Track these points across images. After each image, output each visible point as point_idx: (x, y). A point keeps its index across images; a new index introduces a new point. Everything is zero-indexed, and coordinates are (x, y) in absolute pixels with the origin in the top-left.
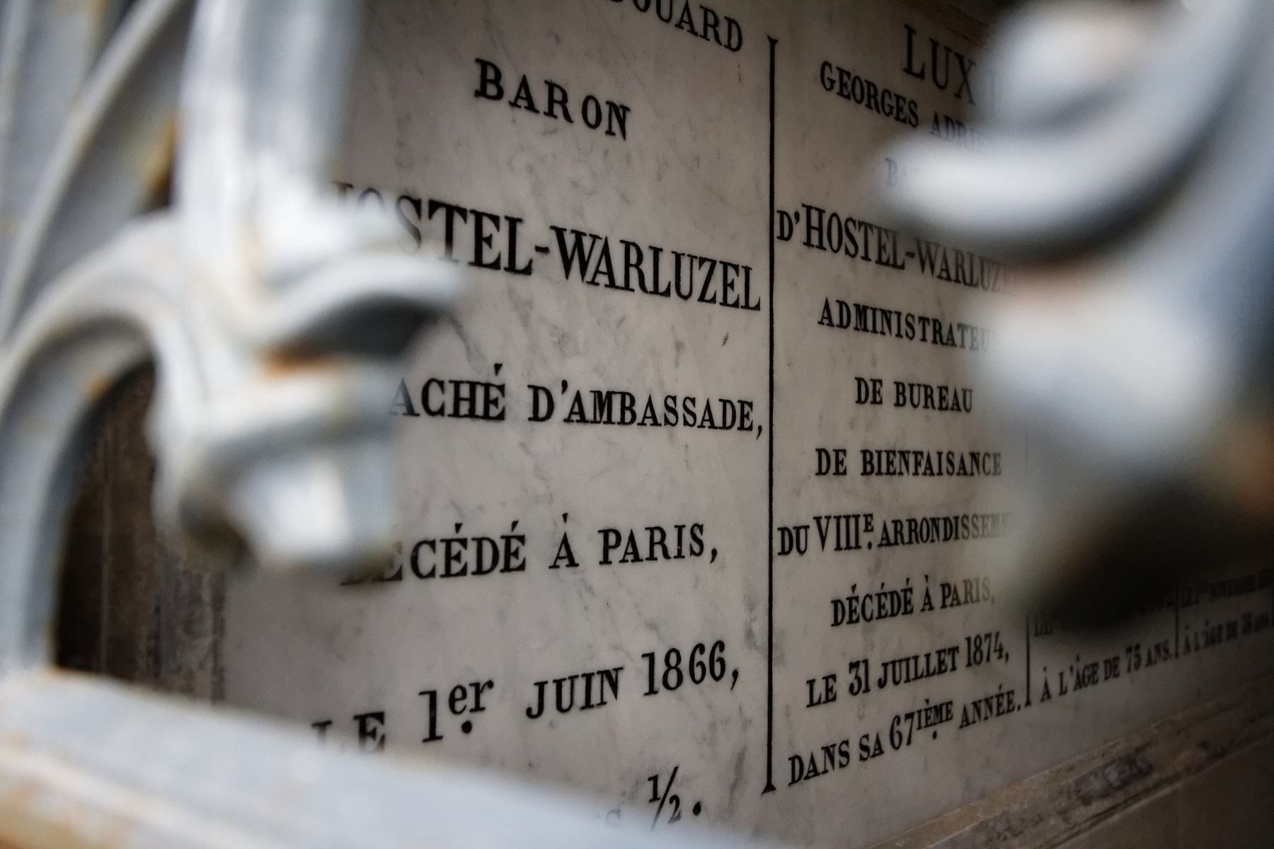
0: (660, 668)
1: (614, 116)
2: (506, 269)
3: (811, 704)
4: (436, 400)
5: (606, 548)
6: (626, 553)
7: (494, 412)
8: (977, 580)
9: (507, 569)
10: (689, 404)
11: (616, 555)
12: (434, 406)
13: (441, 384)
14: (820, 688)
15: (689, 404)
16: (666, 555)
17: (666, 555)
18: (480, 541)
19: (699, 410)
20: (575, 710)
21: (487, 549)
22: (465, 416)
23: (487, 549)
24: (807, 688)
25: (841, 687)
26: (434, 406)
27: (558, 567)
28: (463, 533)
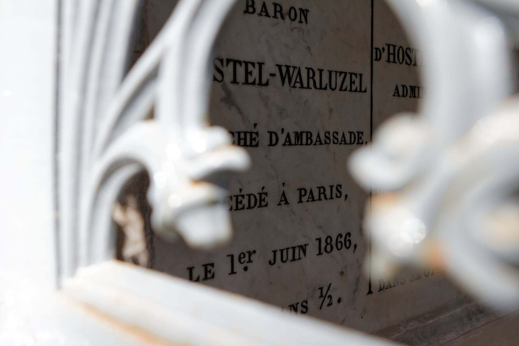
0: (323, 244)
5: (301, 196)
6: (309, 198)
7: (254, 143)
10: (335, 135)
11: (304, 199)
15: (335, 135)
16: (326, 198)
17: (326, 198)
19: (340, 137)
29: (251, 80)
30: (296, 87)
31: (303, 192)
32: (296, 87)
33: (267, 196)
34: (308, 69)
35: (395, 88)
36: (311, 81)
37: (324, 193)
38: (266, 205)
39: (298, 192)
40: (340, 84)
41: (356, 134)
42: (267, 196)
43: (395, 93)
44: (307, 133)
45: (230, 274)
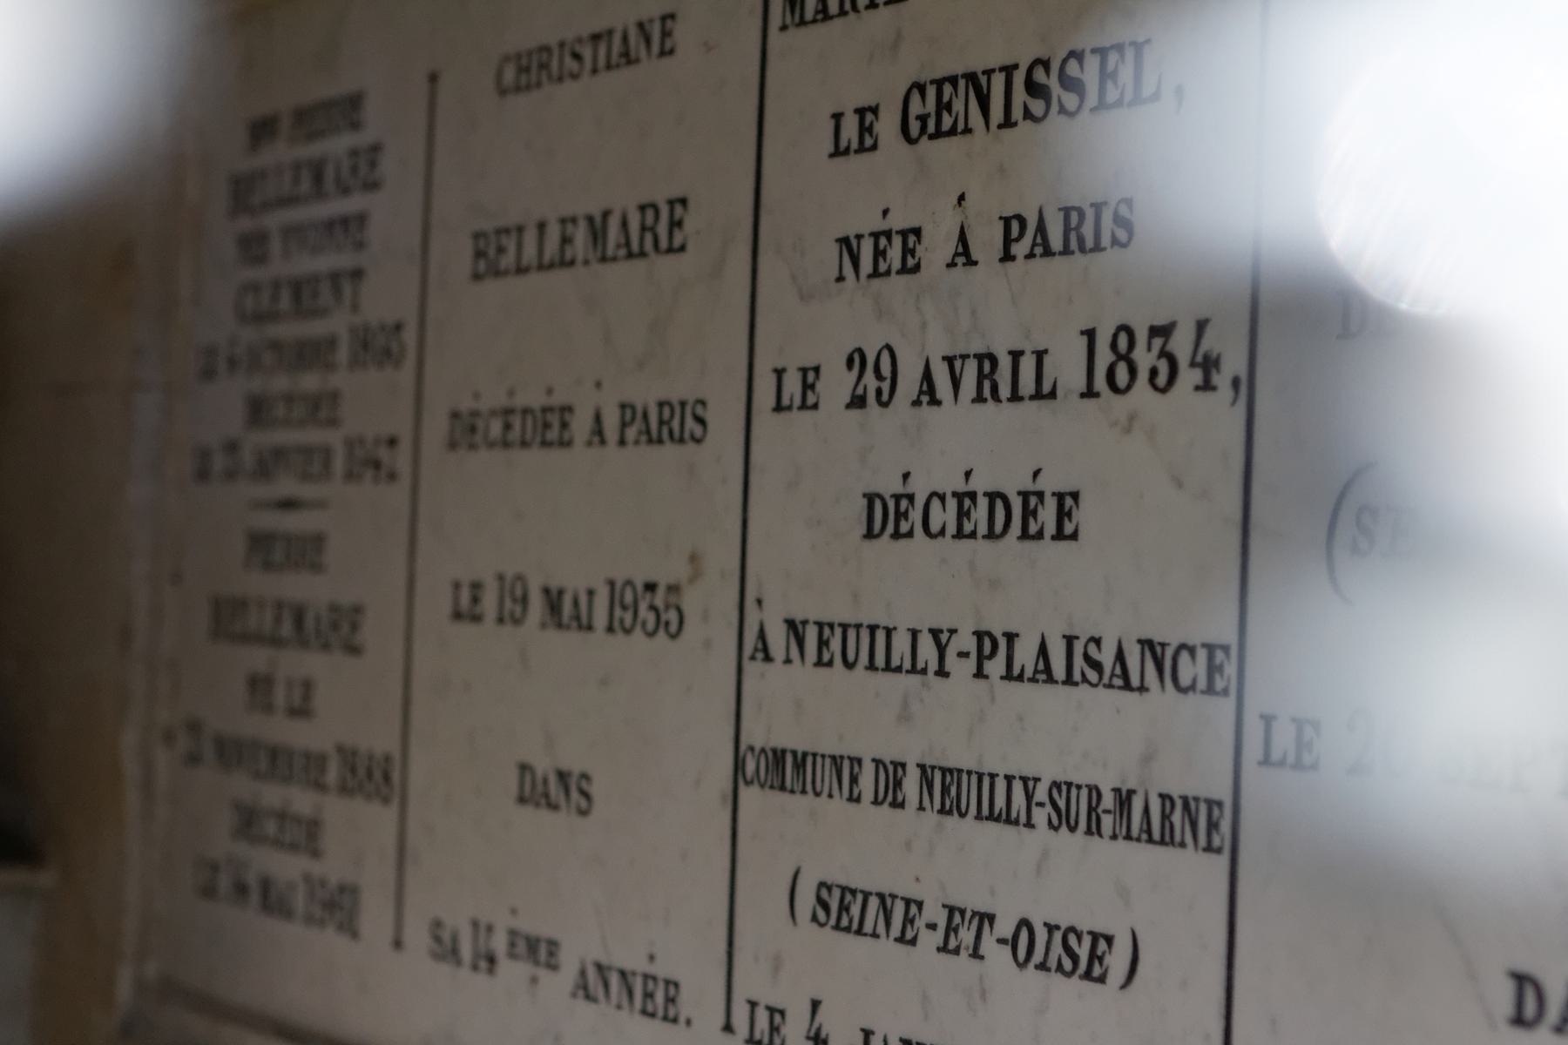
0: (1104, 357)
2: (1009, 400)
5: (1008, 241)
6: (1034, 245)
8: (1098, 207)
10: (1092, 649)
11: (1020, 249)
12: (935, 526)
13: (942, 498)
15: (1092, 649)
19: (1107, 657)
24: (832, 123)
25: (887, 127)
31: (1015, 226)
34: (1163, 796)
35: (1038, 641)
36: (649, 237)
39: (1000, 225)
40: (1064, 662)
41: (539, 415)
43: (921, 392)
44: (1090, 788)
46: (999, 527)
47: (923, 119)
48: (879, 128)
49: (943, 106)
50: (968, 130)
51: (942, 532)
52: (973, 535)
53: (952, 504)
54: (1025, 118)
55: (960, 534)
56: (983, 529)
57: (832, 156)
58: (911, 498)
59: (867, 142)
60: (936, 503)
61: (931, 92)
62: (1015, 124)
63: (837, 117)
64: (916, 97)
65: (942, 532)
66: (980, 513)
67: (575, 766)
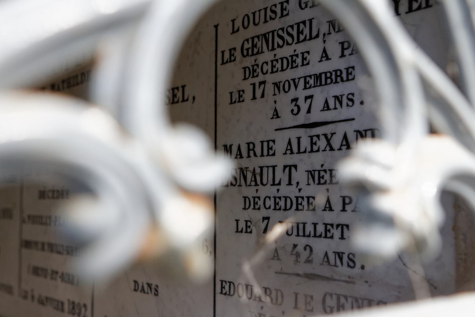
1: (276, 87)
3: (231, 103)
4: (268, 203)
7: (271, 152)
9: (292, 68)
12: (267, 206)
13: (270, 198)
14: (236, 96)
16: (255, 155)
17: (255, 155)
18: (282, 59)
20: (269, 186)
21: (285, 61)
22: (345, 81)
23: (285, 61)
24: (214, 29)
25: (238, 54)
26: (267, 206)
27: (342, 149)
28: (276, 58)
29: (224, 292)
30: (345, 56)
32: (345, 56)
33: (309, 54)
37: (253, 150)
38: (274, 154)
42: (309, 54)
45: (276, 166)
46: (288, 206)
47: (247, 50)
48: (236, 54)
49: (254, 46)
50: (262, 52)
51: (269, 208)
52: (280, 209)
53: (272, 199)
54: (278, 48)
55: (275, 209)
56: (283, 207)
57: (230, 104)
58: (259, 198)
59: (241, 100)
60: (267, 199)
61: (250, 41)
62: (275, 49)
63: (231, 93)
64: (246, 42)
65: (269, 208)
66: (282, 203)
67: (154, 283)
